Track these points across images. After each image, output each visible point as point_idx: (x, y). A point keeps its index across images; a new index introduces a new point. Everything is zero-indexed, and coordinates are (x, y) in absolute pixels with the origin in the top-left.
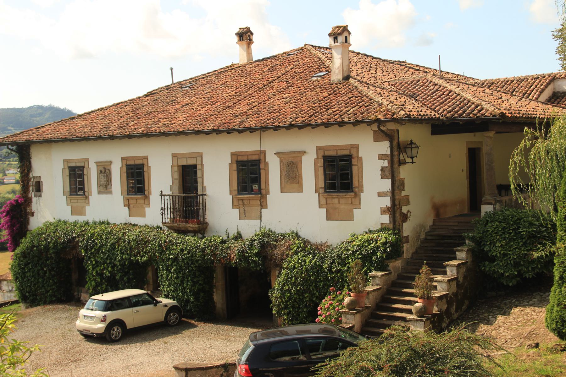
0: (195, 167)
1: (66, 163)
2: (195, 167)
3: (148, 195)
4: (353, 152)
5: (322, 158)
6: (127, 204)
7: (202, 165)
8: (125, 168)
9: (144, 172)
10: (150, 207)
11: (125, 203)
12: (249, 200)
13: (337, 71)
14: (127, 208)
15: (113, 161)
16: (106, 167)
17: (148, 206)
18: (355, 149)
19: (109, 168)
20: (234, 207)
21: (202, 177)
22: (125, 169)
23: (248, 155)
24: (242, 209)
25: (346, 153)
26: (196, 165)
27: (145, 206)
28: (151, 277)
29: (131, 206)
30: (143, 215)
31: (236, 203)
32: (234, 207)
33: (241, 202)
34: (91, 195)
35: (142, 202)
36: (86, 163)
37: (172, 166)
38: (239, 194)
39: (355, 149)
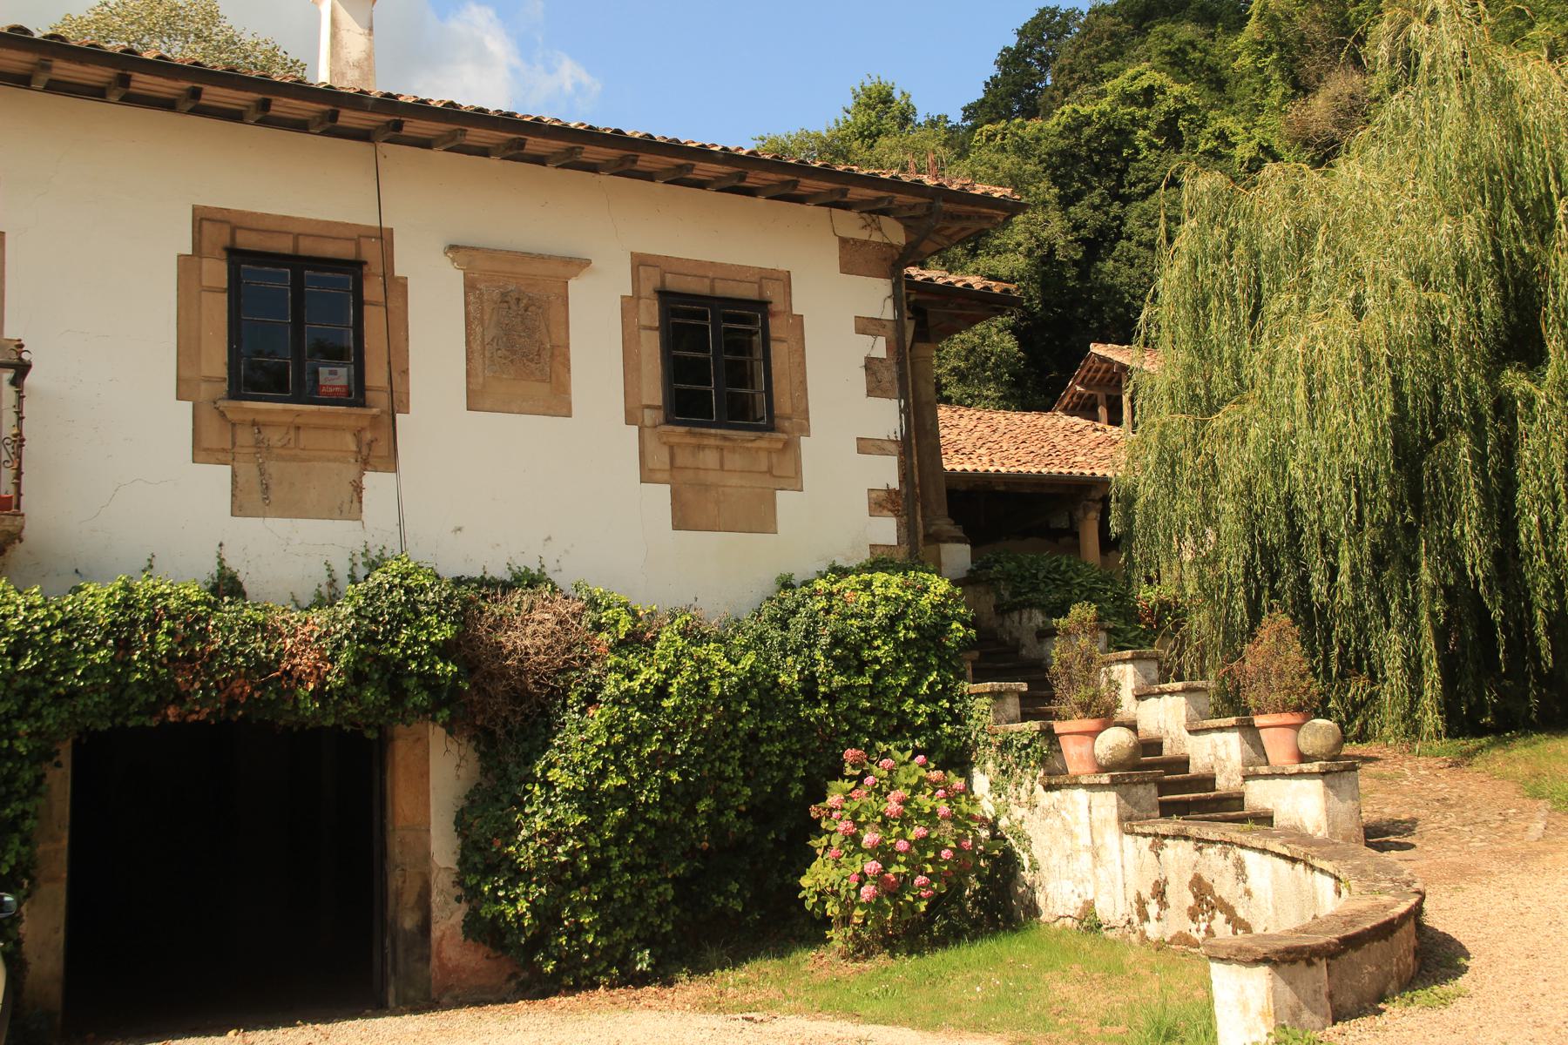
12: (298, 428)
24: (249, 471)
31: (215, 436)
32: (202, 451)
33: (246, 437)
38: (235, 393)
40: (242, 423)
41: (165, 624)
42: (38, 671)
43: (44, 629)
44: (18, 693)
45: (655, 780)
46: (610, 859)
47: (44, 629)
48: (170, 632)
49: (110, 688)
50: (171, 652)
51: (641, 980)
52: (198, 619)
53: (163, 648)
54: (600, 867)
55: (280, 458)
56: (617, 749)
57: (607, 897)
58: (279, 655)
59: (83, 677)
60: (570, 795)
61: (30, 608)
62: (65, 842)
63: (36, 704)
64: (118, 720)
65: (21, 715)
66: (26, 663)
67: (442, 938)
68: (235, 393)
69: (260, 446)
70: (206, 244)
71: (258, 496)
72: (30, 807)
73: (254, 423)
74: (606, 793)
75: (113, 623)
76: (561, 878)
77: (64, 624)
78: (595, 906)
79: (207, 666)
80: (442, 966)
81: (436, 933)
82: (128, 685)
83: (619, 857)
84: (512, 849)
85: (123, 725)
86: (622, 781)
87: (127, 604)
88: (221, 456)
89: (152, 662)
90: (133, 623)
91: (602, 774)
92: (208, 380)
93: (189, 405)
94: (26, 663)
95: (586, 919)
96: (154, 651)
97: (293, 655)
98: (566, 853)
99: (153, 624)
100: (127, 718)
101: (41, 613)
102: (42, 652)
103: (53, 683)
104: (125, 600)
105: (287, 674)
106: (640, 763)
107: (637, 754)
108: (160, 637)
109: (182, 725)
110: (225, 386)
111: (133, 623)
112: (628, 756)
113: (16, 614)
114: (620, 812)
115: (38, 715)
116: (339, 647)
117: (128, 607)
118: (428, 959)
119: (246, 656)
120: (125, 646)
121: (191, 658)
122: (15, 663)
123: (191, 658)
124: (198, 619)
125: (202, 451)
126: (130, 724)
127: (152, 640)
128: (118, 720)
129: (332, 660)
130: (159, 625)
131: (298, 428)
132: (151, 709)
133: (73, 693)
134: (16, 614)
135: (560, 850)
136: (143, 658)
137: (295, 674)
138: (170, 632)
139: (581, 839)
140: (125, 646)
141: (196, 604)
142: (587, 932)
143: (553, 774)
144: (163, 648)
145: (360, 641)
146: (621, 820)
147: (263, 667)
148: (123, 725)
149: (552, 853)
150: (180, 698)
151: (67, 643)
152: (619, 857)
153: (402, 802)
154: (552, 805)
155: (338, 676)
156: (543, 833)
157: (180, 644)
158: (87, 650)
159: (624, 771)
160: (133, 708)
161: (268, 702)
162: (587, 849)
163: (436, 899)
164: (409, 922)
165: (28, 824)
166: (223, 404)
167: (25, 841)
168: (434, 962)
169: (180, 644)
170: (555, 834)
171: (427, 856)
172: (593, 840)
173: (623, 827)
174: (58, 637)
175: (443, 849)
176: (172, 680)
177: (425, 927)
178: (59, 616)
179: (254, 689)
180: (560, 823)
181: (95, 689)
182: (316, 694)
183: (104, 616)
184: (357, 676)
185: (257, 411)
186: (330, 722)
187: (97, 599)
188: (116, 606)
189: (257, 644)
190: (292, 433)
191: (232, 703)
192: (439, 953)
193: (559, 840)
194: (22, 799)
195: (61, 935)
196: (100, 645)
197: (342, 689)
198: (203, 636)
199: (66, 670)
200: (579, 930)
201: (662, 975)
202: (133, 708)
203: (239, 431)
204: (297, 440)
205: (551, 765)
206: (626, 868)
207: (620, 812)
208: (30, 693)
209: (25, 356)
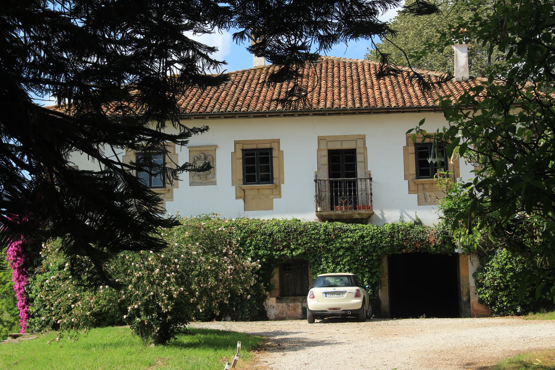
0: (353, 152)
1: (323, 143)
2: (353, 152)
3: (278, 184)
4: (274, 146)
5: (241, 151)
6: (242, 195)
7: (365, 148)
8: (241, 154)
9: (272, 157)
10: (280, 197)
11: (239, 195)
12: (432, 184)
13: (462, 70)
14: (241, 201)
15: (218, 145)
16: (205, 152)
17: (278, 196)
18: (276, 144)
19: (211, 153)
20: (411, 192)
21: (365, 162)
22: (240, 154)
23: (341, 141)
24: (421, 195)
25: (268, 146)
26: (355, 150)
27: (271, 197)
28: (278, 281)
29: (248, 198)
30: (270, 207)
31: (413, 188)
32: (410, 191)
33: (420, 187)
34: (177, 187)
35: (268, 192)
36: (360, 142)
37: (319, 150)
38: (417, 178)
39: (276, 144)
40: (420, 184)
41: (401, 232)
42: (376, 242)
43: (377, 234)
44: (373, 247)
45: (520, 266)
46: (509, 285)
47: (377, 234)
48: (402, 234)
49: (390, 246)
50: (402, 238)
51: (518, 315)
52: (408, 231)
53: (400, 237)
54: (507, 287)
55: (428, 191)
56: (509, 259)
57: (509, 294)
58: (426, 238)
59: (385, 244)
60: (498, 269)
61: (374, 230)
62: (387, 278)
63: (376, 249)
64: (393, 252)
65: (374, 252)
66: (374, 241)
67: (473, 303)
68: (417, 178)
69: (424, 189)
70: (409, 144)
71: (424, 200)
72: (377, 270)
73: (422, 184)
74: (507, 269)
75: (390, 232)
76: (497, 289)
77: (381, 233)
78: (506, 296)
79: (410, 241)
80: (474, 309)
81: (472, 301)
82: (394, 245)
83: (512, 284)
84: (484, 282)
85: (394, 253)
86: (511, 266)
87: (393, 228)
88: (415, 192)
89: (398, 240)
90: (394, 232)
91: (506, 264)
92: (411, 175)
93: (407, 181)
94: (374, 241)
95: (504, 299)
96: (399, 238)
97: (429, 238)
98: (497, 283)
99: (398, 232)
100: (395, 252)
101: (376, 231)
102: (377, 239)
103: (379, 245)
104: (393, 227)
105: (428, 242)
106: (516, 262)
107: (515, 260)
108: (400, 235)
109: (406, 254)
110: (415, 176)
111: (394, 232)
112: (513, 260)
113: (371, 231)
114: (511, 274)
115: (377, 252)
116: (439, 236)
117: (393, 229)
118: (470, 308)
119: (419, 239)
120: (393, 237)
121: (407, 239)
122: (371, 241)
123: (407, 239)
124: (408, 231)
125: (410, 191)
126: (396, 253)
127: (398, 236)
128: (393, 252)
129: (438, 239)
130: (399, 233)
131: (432, 184)
132: (400, 250)
133: (383, 247)
134: (371, 231)
135: (495, 282)
136: (397, 240)
137: (430, 242)
138: (402, 234)
139: (501, 279)
140: (393, 237)
141: (407, 227)
142: (505, 302)
143: (493, 264)
144: (400, 237)
145: (444, 234)
146: (511, 275)
147: (422, 241)
148: (394, 253)
149: (494, 283)
150: (405, 247)
151: (381, 237)
152: (512, 284)
153: (462, 271)
154: (494, 271)
155: (439, 242)
156: (491, 278)
157: (404, 236)
158: (385, 238)
159: (512, 264)
160: (396, 250)
161: (424, 248)
162: (503, 282)
163: (471, 294)
164: (465, 299)
165: (378, 273)
166: (414, 180)
167: (378, 277)
168: (471, 308)
169: (404, 236)
170: (494, 279)
171: (469, 284)
172: (504, 281)
173: (511, 277)
174: (379, 236)
175: (472, 282)
176: (403, 244)
177: (469, 300)
178: (380, 231)
179: (421, 245)
180: (495, 276)
181: (387, 246)
182: (435, 246)
183: (388, 231)
184: (444, 242)
185: (422, 181)
186: (439, 252)
187: (387, 228)
188: (391, 229)
189: (421, 236)
190: (431, 185)
191: (417, 249)
192: (473, 306)
193: (495, 280)
194: (375, 268)
195: (388, 298)
196: (388, 237)
197: (440, 245)
198: (409, 234)
199: (381, 242)
200: (503, 302)
201: (524, 313)
202: (396, 250)
203: (419, 186)
204: (432, 186)
205: (493, 262)
206: (514, 287)
207: (511, 274)
208: (375, 247)
209: (371, 176)
